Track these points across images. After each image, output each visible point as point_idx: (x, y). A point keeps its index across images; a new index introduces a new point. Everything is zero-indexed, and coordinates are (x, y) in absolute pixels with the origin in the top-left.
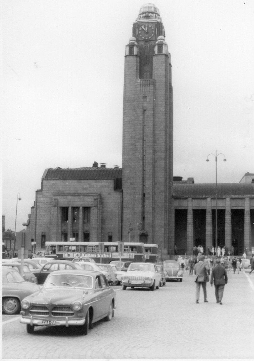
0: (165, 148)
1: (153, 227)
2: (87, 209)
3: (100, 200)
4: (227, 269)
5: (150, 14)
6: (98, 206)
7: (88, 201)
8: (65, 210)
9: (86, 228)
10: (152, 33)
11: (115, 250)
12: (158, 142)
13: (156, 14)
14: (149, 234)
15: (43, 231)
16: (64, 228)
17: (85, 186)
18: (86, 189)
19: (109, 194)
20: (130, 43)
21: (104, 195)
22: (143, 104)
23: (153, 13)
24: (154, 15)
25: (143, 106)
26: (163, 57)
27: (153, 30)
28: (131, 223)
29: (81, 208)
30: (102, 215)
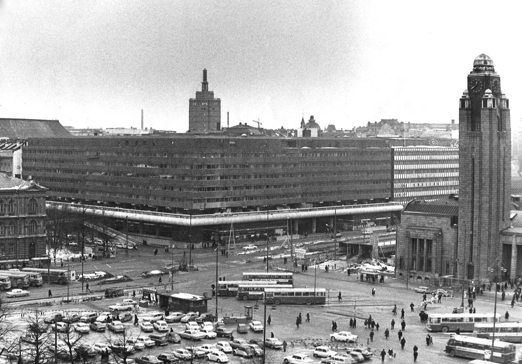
0: (490, 193)
1: (478, 260)
2: (429, 242)
3: (440, 235)
4: (481, 282)
5: (480, 67)
6: (437, 240)
7: (430, 235)
8: (414, 240)
9: (429, 256)
10: (479, 89)
11: (501, 297)
12: (484, 187)
13: (486, 66)
14: (474, 265)
15: (355, 329)
16: (414, 255)
17: (430, 222)
18: (431, 224)
19: (448, 229)
20: (462, 97)
21: (444, 230)
22: (472, 153)
23: (483, 66)
24: (484, 68)
25: (472, 156)
26: (488, 111)
27: (481, 84)
28: (84, 259)
29: (425, 240)
30: (442, 246)
